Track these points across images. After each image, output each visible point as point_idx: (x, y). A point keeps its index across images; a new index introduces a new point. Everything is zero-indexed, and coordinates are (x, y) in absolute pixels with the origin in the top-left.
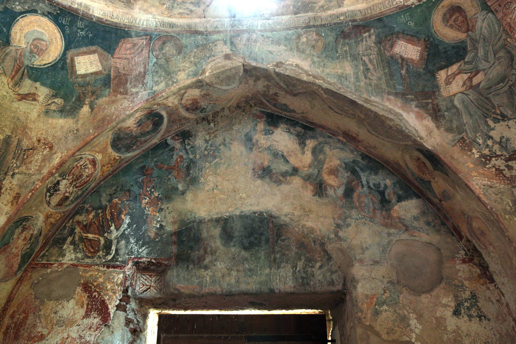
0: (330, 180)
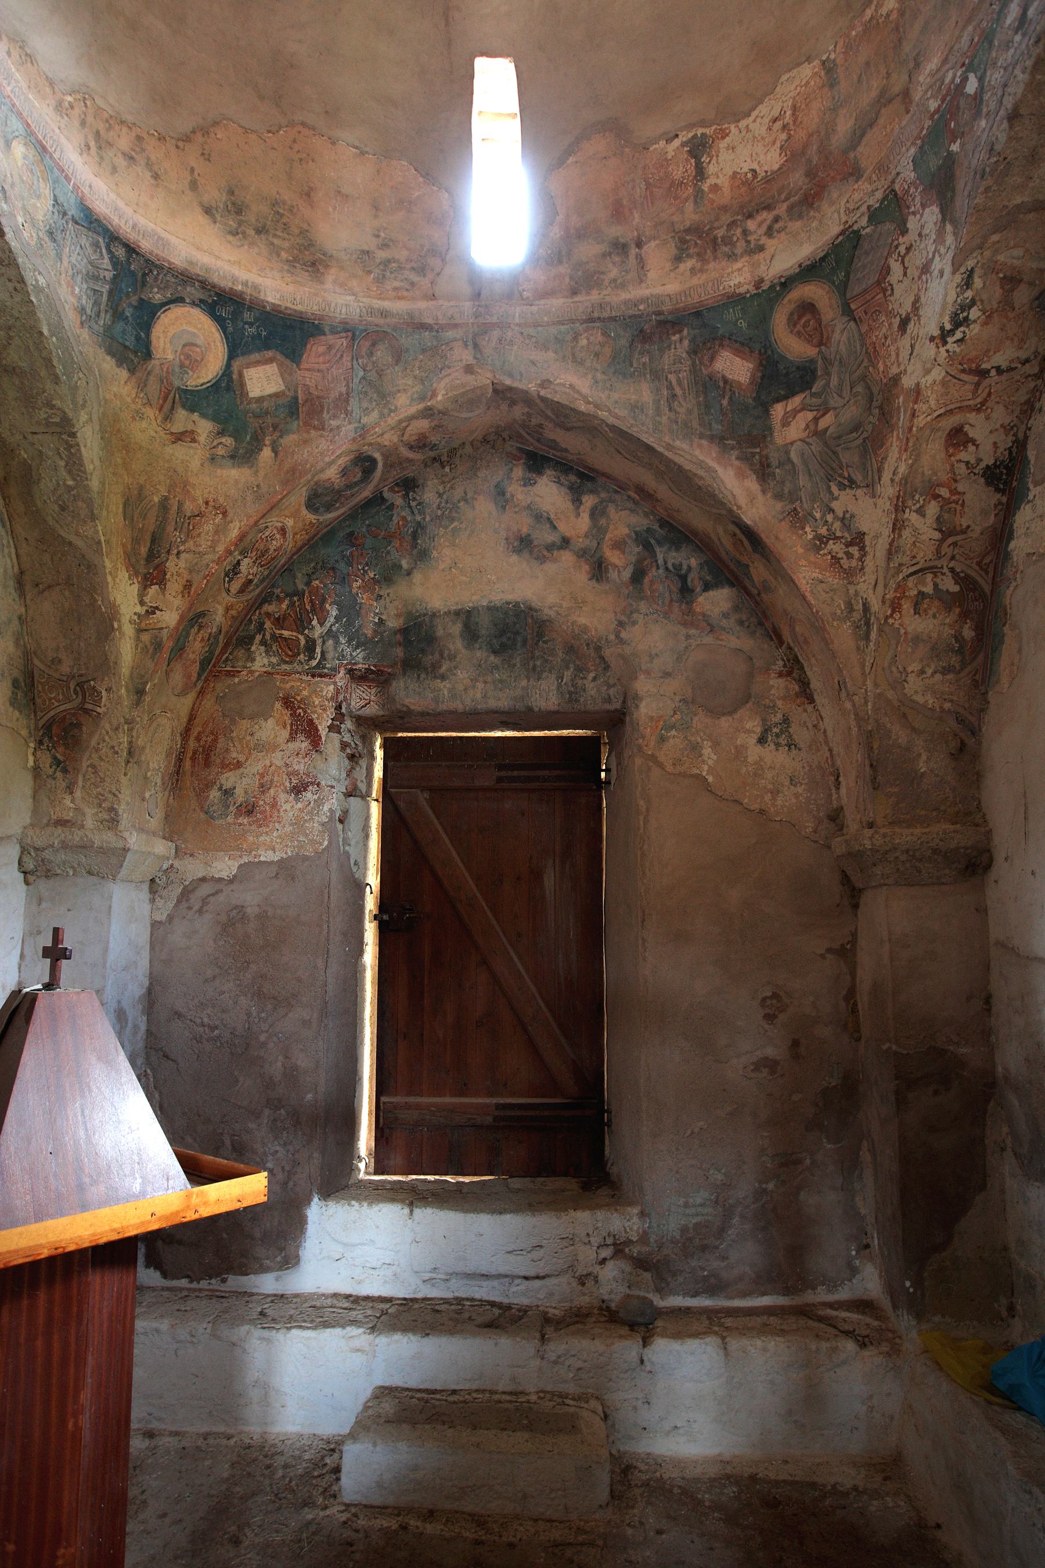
0: (614, 557)
